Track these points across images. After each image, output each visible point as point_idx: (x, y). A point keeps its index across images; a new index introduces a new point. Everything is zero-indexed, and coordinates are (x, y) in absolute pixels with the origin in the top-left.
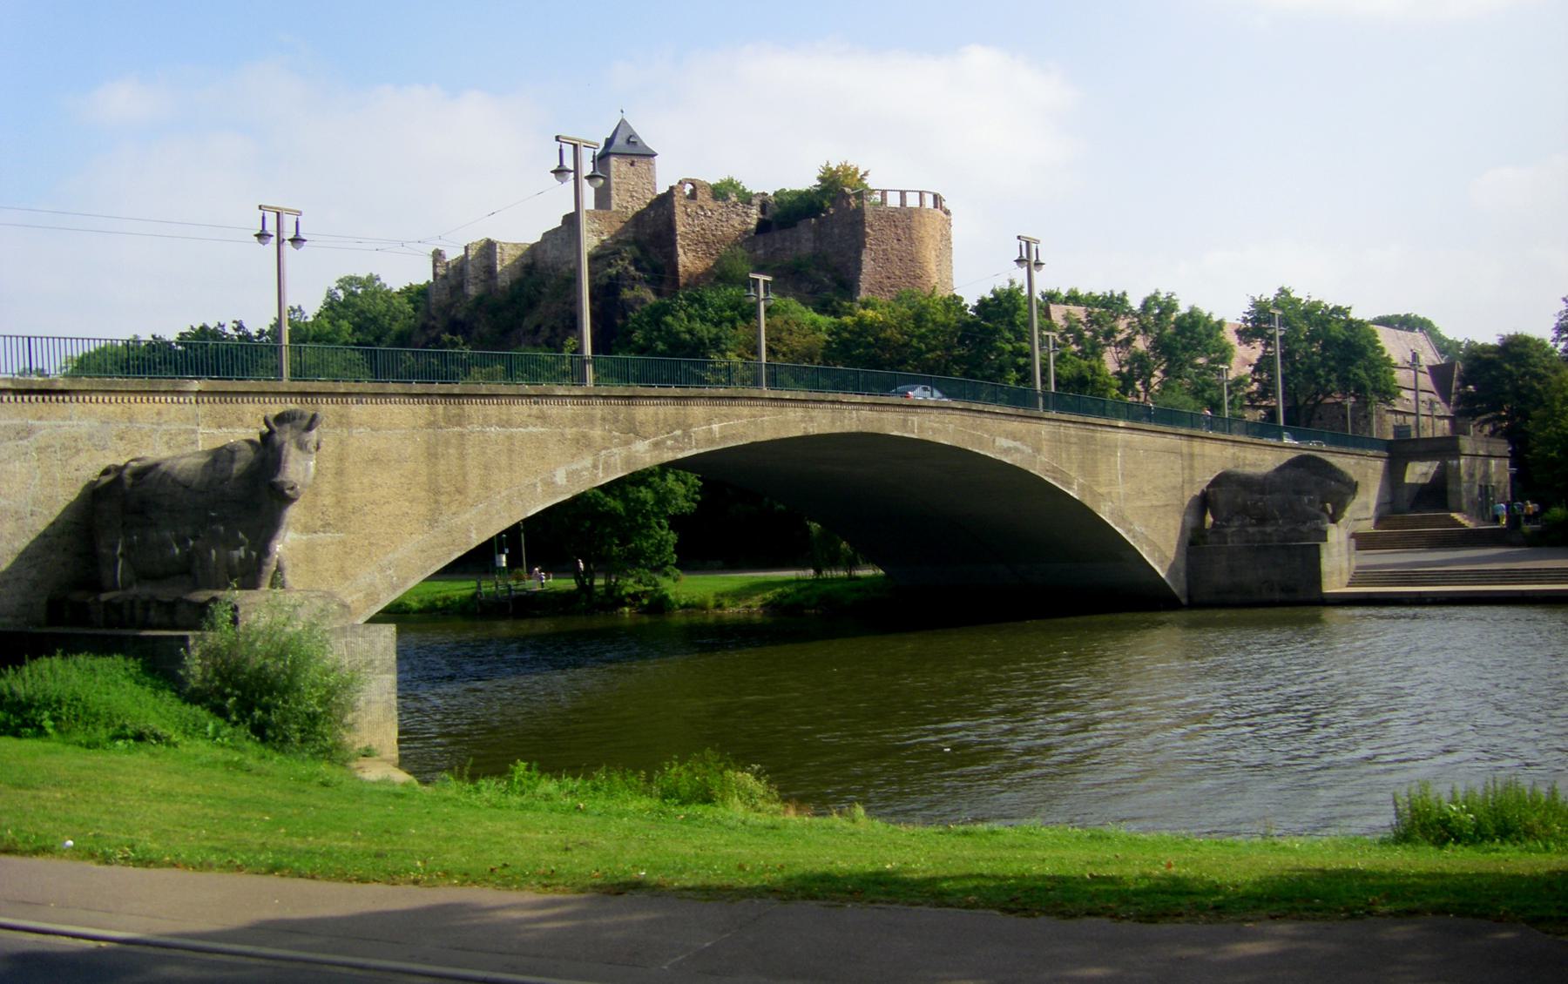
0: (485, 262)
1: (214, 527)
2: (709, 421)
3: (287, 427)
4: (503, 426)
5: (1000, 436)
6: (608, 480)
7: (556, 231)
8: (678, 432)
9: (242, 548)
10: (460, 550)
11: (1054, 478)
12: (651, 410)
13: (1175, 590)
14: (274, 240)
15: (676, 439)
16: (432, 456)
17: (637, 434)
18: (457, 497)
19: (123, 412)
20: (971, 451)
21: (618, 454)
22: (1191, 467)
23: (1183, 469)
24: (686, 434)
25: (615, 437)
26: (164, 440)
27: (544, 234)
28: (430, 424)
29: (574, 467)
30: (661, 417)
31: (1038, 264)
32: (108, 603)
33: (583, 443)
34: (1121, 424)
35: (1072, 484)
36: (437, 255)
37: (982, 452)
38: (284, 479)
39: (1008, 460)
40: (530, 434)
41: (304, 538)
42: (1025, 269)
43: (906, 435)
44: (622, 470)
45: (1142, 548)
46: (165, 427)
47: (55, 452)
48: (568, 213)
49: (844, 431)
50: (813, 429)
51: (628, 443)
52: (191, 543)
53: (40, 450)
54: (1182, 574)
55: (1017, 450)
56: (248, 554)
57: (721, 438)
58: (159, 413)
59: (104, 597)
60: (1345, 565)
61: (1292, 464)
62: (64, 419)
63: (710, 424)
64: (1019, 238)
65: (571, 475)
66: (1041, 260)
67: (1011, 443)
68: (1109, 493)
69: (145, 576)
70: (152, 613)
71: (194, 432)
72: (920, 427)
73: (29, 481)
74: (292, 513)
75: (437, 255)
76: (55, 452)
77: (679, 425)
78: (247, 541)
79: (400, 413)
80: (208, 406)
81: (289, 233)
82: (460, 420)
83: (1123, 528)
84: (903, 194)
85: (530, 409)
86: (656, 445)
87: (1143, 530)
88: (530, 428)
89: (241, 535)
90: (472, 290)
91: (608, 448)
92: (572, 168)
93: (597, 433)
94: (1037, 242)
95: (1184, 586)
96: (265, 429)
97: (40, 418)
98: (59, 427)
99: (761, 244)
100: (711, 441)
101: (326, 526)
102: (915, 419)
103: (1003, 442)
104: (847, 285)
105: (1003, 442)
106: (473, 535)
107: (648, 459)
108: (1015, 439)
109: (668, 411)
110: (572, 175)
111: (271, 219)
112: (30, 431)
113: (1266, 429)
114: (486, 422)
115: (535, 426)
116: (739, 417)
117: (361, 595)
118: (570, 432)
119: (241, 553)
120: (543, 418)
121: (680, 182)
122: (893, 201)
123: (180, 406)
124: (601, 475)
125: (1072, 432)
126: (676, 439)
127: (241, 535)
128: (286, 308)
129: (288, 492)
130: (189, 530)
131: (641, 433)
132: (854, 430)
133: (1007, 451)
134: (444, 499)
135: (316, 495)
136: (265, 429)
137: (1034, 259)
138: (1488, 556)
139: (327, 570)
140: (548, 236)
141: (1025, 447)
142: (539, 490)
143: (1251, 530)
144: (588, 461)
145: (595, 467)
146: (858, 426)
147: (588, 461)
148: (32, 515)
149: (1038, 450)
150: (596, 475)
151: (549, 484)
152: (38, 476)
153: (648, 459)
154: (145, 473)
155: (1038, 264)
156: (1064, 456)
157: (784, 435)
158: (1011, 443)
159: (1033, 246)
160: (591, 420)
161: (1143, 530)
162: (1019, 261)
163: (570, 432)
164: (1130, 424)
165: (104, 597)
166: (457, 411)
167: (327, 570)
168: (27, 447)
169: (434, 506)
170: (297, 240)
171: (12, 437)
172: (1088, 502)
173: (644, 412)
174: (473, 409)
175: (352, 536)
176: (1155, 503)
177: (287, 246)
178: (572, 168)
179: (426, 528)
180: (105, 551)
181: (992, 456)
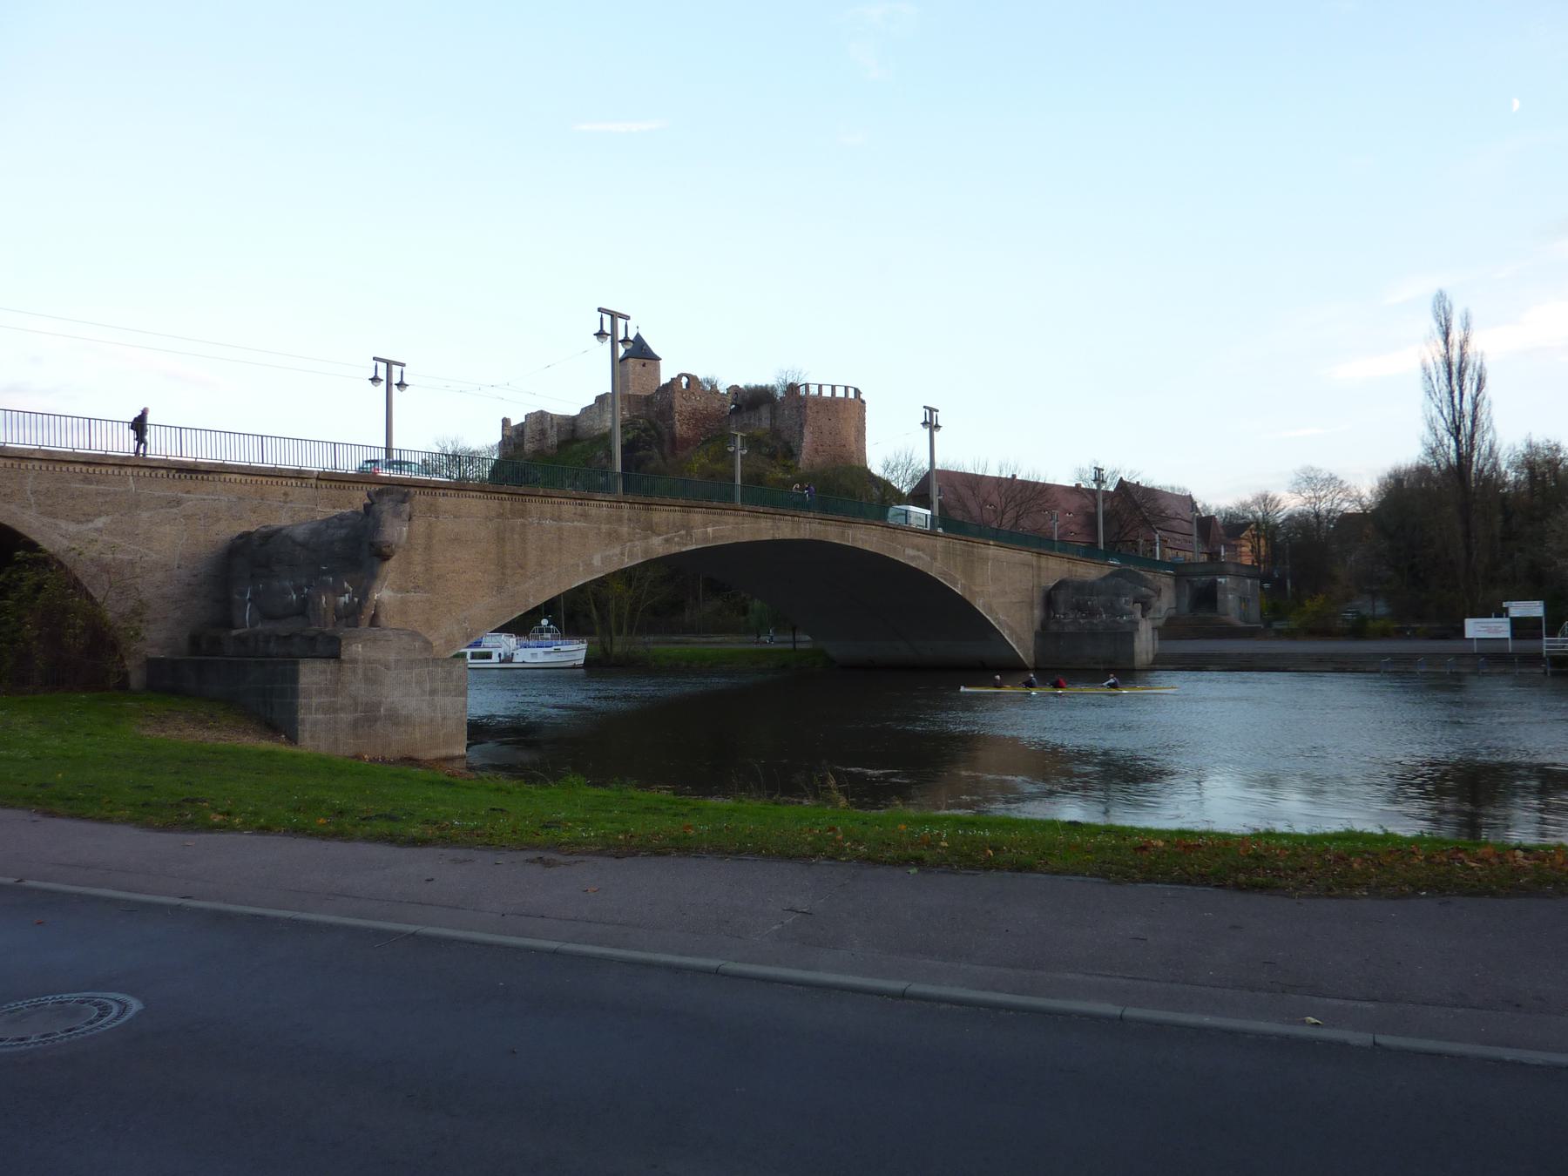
0: (540, 427)
1: (324, 578)
2: (705, 526)
3: (386, 498)
4: (555, 521)
5: (908, 547)
6: (632, 564)
7: (591, 407)
8: (683, 532)
9: (347, 595)
10: (520, 611)
11: (945, 579)
12: (664, 514)
13: (1026, 662)
14: (384, 384)
15: (681, 537)
16: (500, 539)
17: (653, 532)
18: (519, 571)
19: (256, 492)
20: (893, 559)
21: (639, 546)
22: (1039, 576)
23: (1033, 577)
24: (689, 534)
25: (637, 533)
26: (290, 514)
27: (582, 409)
28: (500, 515)
29: (607, 553)
30: (672, 519)
31: (937, 427)
32: (238, 637)
33: (613, 537)
34: (991, 543)
35: (957, 583)
36: (505, 422)
37: (896, 558)
38: (382, 540)
39: (913, 565)
40: (575, 527)
41: (400, 596)
42: (928, 429)
43: (843, 543)
44: (642, 557)
45: (1004, 631)
46: (289, 505)
47: (200, 519)
48: (599, 394)
49: (801, 538)
50: (780, 536)
51: (646, 538)
52: (306, 590)
53: (186, 517)
54: (1031, 652)
55: (919, 557)
56: (351, 599)
57: (713, 538)
58: (286, 494)
59: (234, 632)
60: (1150, 648)
61: (1112, 575)
62: (208, 494)
63: (706, 527)
64: (925, 407)
65: (604, 560)
66: (939, 424)
67: (917, 553)
68: (982, 591)
69: (269, 617)
70: (272, 645)
71: (313, 509)
72: (853, 539)
73: (177, 541)
74: (390, 568)
75: (505, 422)
76: (200, 519)
77: (683, 527)
78: (351, 589)
79: (476, 505)
80: (325, 490)
81: (396, 379)
82: (523, 514)
83: (991, 616)
84: (833, 388)
85: (576, 509)
86: (667, 541)
87: (1006, 618)
88: (575, 523)
89: (346, 585)
90: (528, 447)
91: (632, 541)
92: (610, 333)
93: (625, 530)
94: (937, 411)
95: (1033, 660)
96: (367, 501)
97: (188, 492)
98: (204, 500)
99: (734, 420)
100: (706, 539)
101: (417, 588)
102: (850, 532)
103: (910, 552)
104: (790, 453)
105: (910, 552)
106: (531, 600)
107: (661, 550)
108: (918, 550)
109: (676, 516)
110: (609, 338)
111: (382, 367)
112: (179, 502)
113: (1090, 552)
114: (542, 517)
115: (579, 521)
116: (727, 524)
117: (443, 641)
118: (604, 528)
119: (345, 599)
120: (585, 516)
121: (679, 376)
122: (827, 393)
123: (303, 490)
124: (626, 560)
125: (958, 547)
126: (681, 537)
127: (346, 585)
128: (412, 490)
129: (384, 549)
130: (304, 581)
131: (657, 531)
132: (807, 537)
133: (913, 558)
134: (508, 572)
135: (410, 563)
136: (367, 501)
137: (935, 423)
138: (1185, 656)
139: (416, 621)
140: (586, 410)
141: (925, 556)
142: (581, 569)
143: (1081, 621)
144: (617, 550)
145: (622, 554)
146: (810, 534)
147: (617, 550)
148: (178, 567)
149: (934, 558)
150: (623, 560)
151: (589, 565)
152: (185, 537)
153: (661, 550)
154: (269, 537)
155: (937, 427)
156: (952, 562)
157: (758, 538)
158: (917, 553)
159: (935, 413)
160: (620, 520)
161: (1006, 618)
162: (924, 424)
163: (604, 528)
164: (997, 543)
165: (234, 632)
166: (521, 507)
167: (416, 621)
168: (176, 514)
169: (501, 576)
170: (401, 385)
171: (164, 505)
172: (967, 597)
173: (660, 516)
174: (533, 506)
175: (437, 596)
176: (1014, 600)
177: (395, 388)
178: (610, 333)
179: (494, 593)
180: (237, 597)
181: (903, 561)
